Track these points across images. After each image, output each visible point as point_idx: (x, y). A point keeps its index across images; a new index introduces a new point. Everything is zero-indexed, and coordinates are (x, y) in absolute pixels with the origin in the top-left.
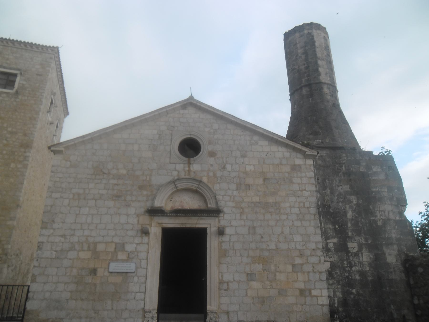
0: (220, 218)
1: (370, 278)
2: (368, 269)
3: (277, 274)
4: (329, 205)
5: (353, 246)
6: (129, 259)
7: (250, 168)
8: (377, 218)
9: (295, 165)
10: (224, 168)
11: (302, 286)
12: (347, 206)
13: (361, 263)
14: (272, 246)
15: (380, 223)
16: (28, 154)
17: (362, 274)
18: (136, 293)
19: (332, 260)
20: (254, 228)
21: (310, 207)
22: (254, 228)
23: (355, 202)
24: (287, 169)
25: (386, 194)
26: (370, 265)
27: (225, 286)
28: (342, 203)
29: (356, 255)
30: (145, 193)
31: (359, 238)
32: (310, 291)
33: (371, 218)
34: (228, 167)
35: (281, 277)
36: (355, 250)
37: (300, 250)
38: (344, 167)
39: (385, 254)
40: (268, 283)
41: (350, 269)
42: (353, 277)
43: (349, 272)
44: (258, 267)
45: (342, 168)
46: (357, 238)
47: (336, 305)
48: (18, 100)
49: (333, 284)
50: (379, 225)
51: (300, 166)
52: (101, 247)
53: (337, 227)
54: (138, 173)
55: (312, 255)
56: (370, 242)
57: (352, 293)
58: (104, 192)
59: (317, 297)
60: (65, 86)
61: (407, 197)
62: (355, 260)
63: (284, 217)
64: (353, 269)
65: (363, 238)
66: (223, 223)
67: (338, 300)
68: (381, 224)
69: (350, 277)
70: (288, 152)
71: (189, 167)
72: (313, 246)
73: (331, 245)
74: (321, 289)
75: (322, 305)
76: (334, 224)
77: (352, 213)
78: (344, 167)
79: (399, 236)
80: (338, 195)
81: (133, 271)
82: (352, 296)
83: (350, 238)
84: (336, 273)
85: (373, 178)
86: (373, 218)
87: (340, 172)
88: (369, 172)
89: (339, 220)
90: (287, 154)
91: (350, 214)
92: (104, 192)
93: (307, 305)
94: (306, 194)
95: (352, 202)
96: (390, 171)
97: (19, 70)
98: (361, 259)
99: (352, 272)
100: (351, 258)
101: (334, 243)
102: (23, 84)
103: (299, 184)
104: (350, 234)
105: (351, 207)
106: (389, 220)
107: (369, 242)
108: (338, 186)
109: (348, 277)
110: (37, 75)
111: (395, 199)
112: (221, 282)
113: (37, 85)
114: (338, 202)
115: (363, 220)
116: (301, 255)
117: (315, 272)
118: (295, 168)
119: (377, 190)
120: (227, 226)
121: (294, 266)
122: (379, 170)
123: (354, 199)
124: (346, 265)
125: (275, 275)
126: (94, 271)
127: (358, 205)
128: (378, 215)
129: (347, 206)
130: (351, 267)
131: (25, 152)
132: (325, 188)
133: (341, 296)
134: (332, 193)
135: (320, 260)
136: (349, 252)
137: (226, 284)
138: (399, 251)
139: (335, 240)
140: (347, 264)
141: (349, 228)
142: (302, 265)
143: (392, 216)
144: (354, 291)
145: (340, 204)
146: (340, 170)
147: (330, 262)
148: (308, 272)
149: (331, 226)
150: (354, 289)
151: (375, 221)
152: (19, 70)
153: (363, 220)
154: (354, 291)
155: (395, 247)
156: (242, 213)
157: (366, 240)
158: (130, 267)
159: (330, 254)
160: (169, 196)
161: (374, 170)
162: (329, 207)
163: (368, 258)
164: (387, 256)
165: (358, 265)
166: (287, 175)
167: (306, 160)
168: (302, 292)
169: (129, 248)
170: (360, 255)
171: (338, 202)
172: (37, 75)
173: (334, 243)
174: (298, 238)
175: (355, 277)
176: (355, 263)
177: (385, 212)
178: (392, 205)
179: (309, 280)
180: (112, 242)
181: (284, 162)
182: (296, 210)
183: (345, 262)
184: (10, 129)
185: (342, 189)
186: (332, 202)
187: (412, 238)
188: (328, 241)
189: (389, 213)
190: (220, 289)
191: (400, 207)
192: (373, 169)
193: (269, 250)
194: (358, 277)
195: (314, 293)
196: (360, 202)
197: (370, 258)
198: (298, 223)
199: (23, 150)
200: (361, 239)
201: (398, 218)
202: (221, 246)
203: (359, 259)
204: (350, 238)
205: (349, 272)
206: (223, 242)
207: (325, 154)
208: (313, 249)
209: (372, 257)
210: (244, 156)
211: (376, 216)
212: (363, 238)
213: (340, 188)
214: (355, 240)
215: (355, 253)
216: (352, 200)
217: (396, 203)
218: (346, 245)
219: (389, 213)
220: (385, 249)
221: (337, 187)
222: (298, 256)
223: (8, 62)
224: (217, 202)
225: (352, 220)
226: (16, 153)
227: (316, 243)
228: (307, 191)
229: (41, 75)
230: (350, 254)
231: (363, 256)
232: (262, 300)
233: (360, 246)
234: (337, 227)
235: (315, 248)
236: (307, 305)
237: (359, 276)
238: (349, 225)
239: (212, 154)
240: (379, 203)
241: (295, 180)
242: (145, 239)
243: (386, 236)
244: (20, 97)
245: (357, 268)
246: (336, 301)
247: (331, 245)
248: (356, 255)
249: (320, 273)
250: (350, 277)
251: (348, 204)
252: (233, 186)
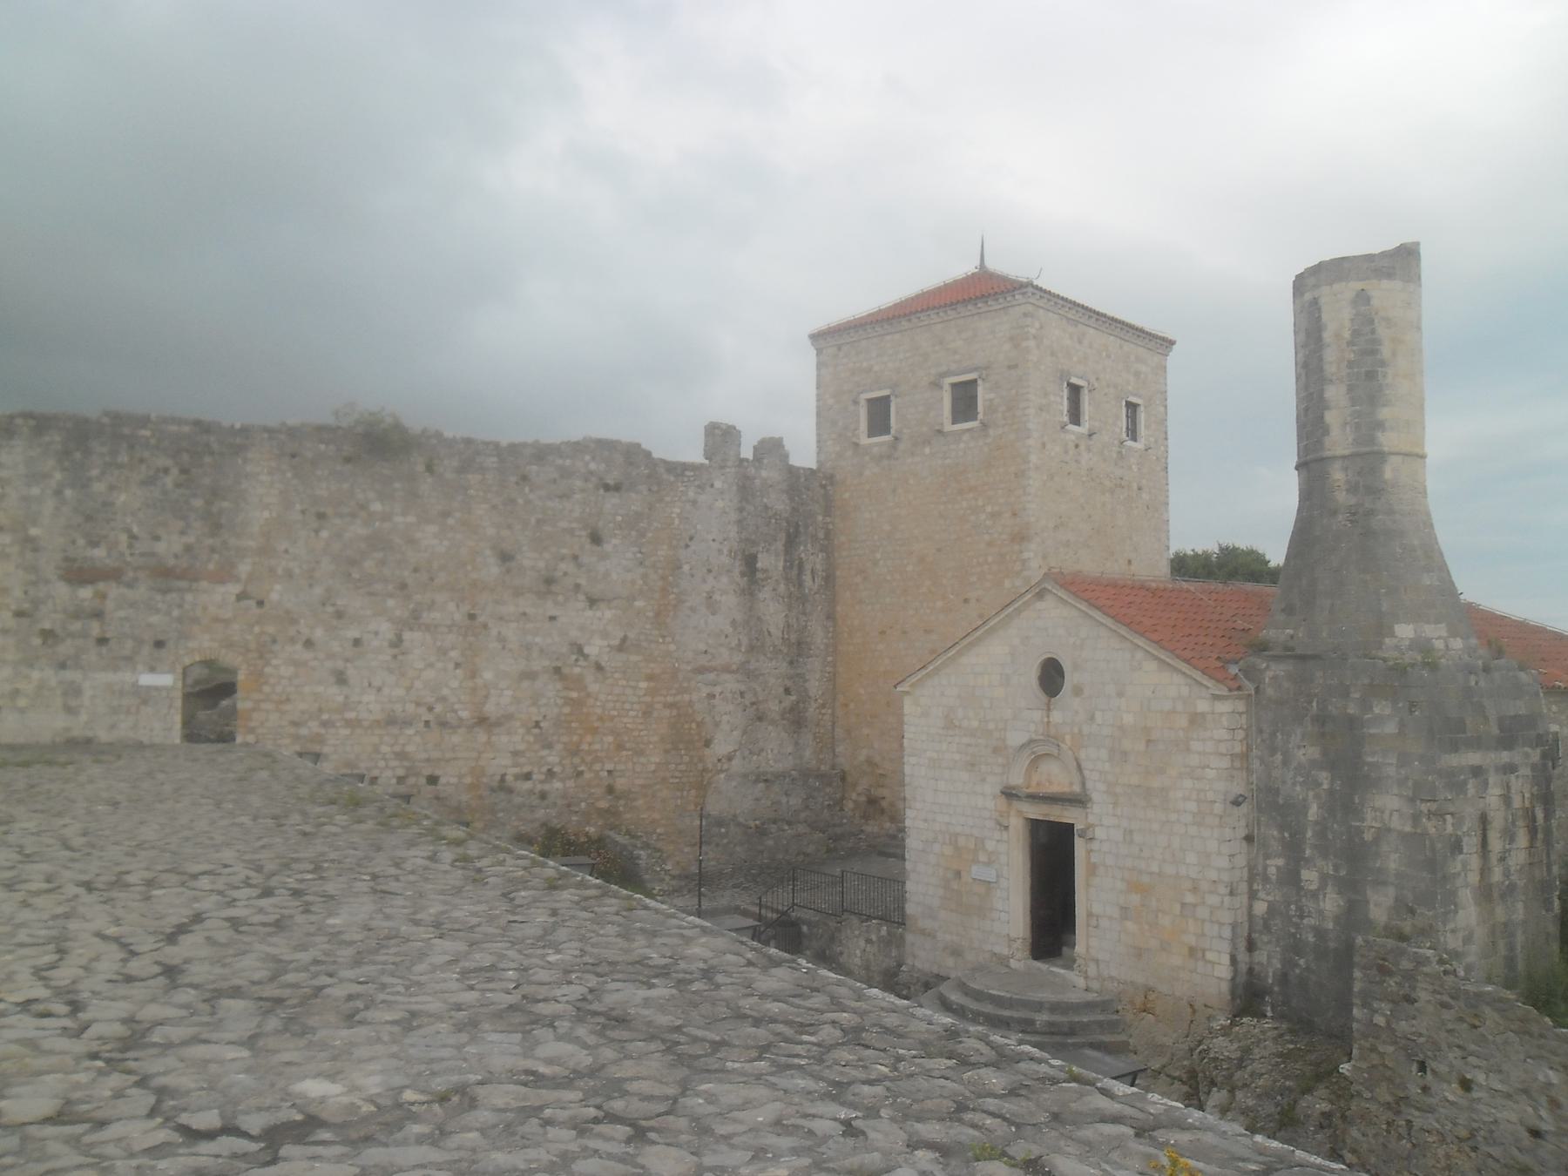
0: (1089, 810)
1: (1332, 945)
2: (1330, 926)
3: (1160, 915)
4: (1278, 788)
5: (1310, 877)
6: (989, 863)
7: (1128, 719)
8: (1364, 824)
9: (1196, 714)
10: (1092, 718)
11: (1191, 940)
12: (1311, 794)
13: (1321, 912)
14: (1155, 868)
15: (1368, 836)
16: (1026, 555)
17: (1320, 933)
18: (60, 1114)
19: (1270, 898)
20: (1131, 832)
21: (1215, 802)
22: (1131, 832)
23: (1325, 786)
24: (1183, 722)
25: (1391, 771)
26: (1337, 919)
27: (1094, 922)
28: (1301, 785)
29: (1314, 895)
30: (1000, 760)
31: (1324, 863)
32: (1204, 951)
33: (1353, 823)
34: (1098, 715)
35: (1165, 921)
36: (1313, 887)
37: (1193, 880)
38: (1314, 704)
39: (1367, 902)
40: (1146, 927)
41: (1299, 921)
42: (1304, 937)
43: (1297, 926)
44: (1135, 899)
45: (1312, 706)
46: (1320, 862)
47: (1270, 981)
48: (989, 440)
49: (1269, 942)
50: (1366, 839)
51: (1203, 715)
52: (962, 841)
53: (1286, 835)
54: (991, 726)
55: (1211, 892)
56: (1343, 873)
57: (1297, 965)
58: (957, 757)
59: (1213, 963)
60: (1110, 313)
61: (1092, 869)
62: (1309, 905)
63: (1173, 817)
64: (1305, 921)
65: (1330, 864)
66: (1091, 819)
67: (1274, 973)
68: (1371, 839)
69: (1298, 936)
70: (1186, 685)
71: (1048, 717)
72: (1213, 875)
73: (1272, 871)
74: (1219, 952)
75: (1220, 979)
76: (1281, 828)
77: (1319, 808)
78: (1314, 704)
79: (1403, 869)
80: (1295, 768)
81: (994, 880)
82: (1297, 971)
83: (1307, 860)
84: (1276, 925)
85: (1372, 731)
86: (1358, 824)
87: (1307, 715)
88: (1366, 716)
89: (1292, 821)
90: (1185, 691)
91: (1313, 812)
92: (957, 757)
93: (1198, 973)
94: (1211, 773)
95: (1321, 784)
96: (1417, 713)
97: (975, 369)
98: (1321, 904)
99: (1302, 926)
100: (1304, 900)
101: (1278, 868)
102: (991, 400)
103: (1199, 753)
104: (1308, 852)
105: (1317, 796)
106: (1389, 830)
107: (1341, 874)
108: (1299, 747)
109: (1294, 935)
110: (1010, 367)
111: (1410, 783)
112: (1090, 915)
113: (1014, 392)
114: (1294, 784)
115: (1335, 826)
116: (1195, 890)
117: (1212, 922)
118: (1196, 719)
119: (1375, 759)
120: (1097, 826)
121: (1183, 905)
122: (1388, 711)
123: (1324, 777)
124: (1293, 913)
125: (1157, 917)
126: (958, 874)
127: (1331, 792)
128: (1369, 815)
129: (1311, 794)
130: (1302, 917)
131: (1021, 552)
132: (1273, 751)
133: (1279, 966)
134: (1285, 763)
135: (1222, 902)
136: (1302, 888)
137: (1095, 918)
138: (1397, 900)
139: (1280, 862)
140: (1296, 911)
141: (1308, 841)
142: (1195, 906)
143: (1395, 823)
144: (1302, 962)
145: (1298, 788)
146: (1307, 710)
147: (1268, 902)
148: (1203, 921)
149: (1275, 833)
150: (1303, 958)
151: (1360, 831)
152: (975, 369)
153: (1335, 826)
154: (1302, 962)
155: (1391, 891)
156: (1115, 804)
157: (1336, 868)
158: (989, 874)
159: (1268, 886)
160: (1027, 770)
161: (1377, 710)
162: (1277, 792)
163: (1335, 904)
164: (1372, 906)
165: (1314, 916)
166: (1181, 734)
167: (1216, 702)
168: (1192, 951)
169: (990, 845)
170: (1321, 897)
171: (1294, 784)
172: (1010, 367)
173: (1278, 868)
174: (1191, 858)
175: (1307, 938)
176: (1309, 912)
177: (1383, 812)
178: (1400, 796)
179: (1203, 935)
180: (972, 835)
181: (1180, 707)
182: (1192, 806)
183: (1293, 907)
184: (989, 509)
185: (1304, 754)
186: (1284, 782)
187: (1429, 876)
188: (1268, 862)
189: (1391, 815)
190: (1088, 925)
191: (1418, 802)
192: (1374, 709)
193: (1151, 874)
194: (1311, 939)
195: (1210, 956)
196: (1338, 785)
197: (1339, 906)
198: (1193, 830)
199: (1016, 547)
200: (1327, 865)
201: (1408, 829)
202: (1089, 858)
203: (1319, 906)
204: (1307, 860)
205: (1297, 926)
206: (1091, 850)
207: (1283, 673)
208: (1214, 881)
209: (1342, 904)
210: (1120, 695)
211: (1363, 820)
212: (1330, 864)
213: (1302, 751)
214: (1315, 867)
215: (1311, 891)
216: (1320, 781)
217: (1411, 794)
218: (1298, 873)
219: (1391, 815)
220: (1369, 892)
221: (1296, 750)
222: (1190, 890)
223: (957, 357)
224: (1083, 784)
225: (1316, 823)
226: (1008, 557)
227: (1219, 870)
228: (1212, 769)
229: (1015, 366)
230: (1302, 893)
231: (1327, 899)
232: (1139, 953)
233: (1324, 878)
234: (1286, 835)
235: (1216, 879)
236: (1198, 973)
237: (1315, 936)
238: (1309, 834)
239: (1078, 691)
240: (1374, 791)
241: (1195, 746)
242: (1005, 835)
243: (1377, 865)
244: (991, 432)
245: (1313, 921)
246: (1271, 974)
247: (1272, 871)
248: (1314, 895)
249: (1221, 924)
250: (1298, 936)
251: (1313, 789)
252: (1104, 754)
